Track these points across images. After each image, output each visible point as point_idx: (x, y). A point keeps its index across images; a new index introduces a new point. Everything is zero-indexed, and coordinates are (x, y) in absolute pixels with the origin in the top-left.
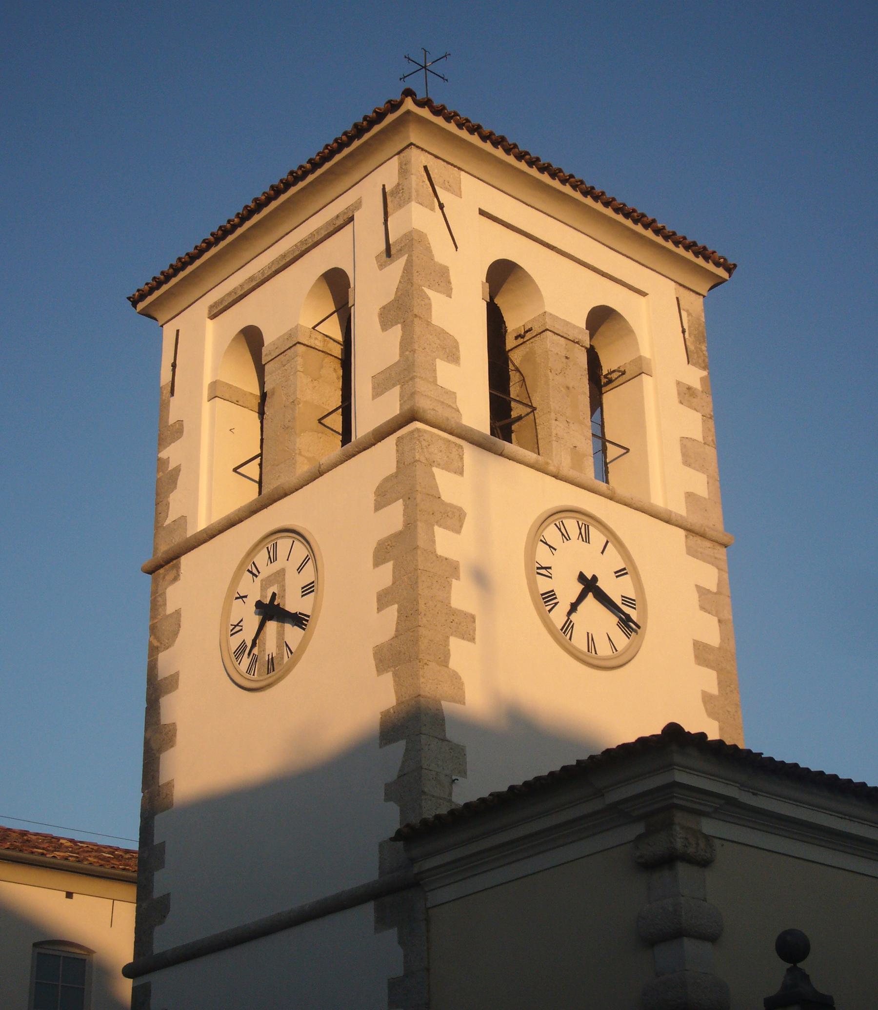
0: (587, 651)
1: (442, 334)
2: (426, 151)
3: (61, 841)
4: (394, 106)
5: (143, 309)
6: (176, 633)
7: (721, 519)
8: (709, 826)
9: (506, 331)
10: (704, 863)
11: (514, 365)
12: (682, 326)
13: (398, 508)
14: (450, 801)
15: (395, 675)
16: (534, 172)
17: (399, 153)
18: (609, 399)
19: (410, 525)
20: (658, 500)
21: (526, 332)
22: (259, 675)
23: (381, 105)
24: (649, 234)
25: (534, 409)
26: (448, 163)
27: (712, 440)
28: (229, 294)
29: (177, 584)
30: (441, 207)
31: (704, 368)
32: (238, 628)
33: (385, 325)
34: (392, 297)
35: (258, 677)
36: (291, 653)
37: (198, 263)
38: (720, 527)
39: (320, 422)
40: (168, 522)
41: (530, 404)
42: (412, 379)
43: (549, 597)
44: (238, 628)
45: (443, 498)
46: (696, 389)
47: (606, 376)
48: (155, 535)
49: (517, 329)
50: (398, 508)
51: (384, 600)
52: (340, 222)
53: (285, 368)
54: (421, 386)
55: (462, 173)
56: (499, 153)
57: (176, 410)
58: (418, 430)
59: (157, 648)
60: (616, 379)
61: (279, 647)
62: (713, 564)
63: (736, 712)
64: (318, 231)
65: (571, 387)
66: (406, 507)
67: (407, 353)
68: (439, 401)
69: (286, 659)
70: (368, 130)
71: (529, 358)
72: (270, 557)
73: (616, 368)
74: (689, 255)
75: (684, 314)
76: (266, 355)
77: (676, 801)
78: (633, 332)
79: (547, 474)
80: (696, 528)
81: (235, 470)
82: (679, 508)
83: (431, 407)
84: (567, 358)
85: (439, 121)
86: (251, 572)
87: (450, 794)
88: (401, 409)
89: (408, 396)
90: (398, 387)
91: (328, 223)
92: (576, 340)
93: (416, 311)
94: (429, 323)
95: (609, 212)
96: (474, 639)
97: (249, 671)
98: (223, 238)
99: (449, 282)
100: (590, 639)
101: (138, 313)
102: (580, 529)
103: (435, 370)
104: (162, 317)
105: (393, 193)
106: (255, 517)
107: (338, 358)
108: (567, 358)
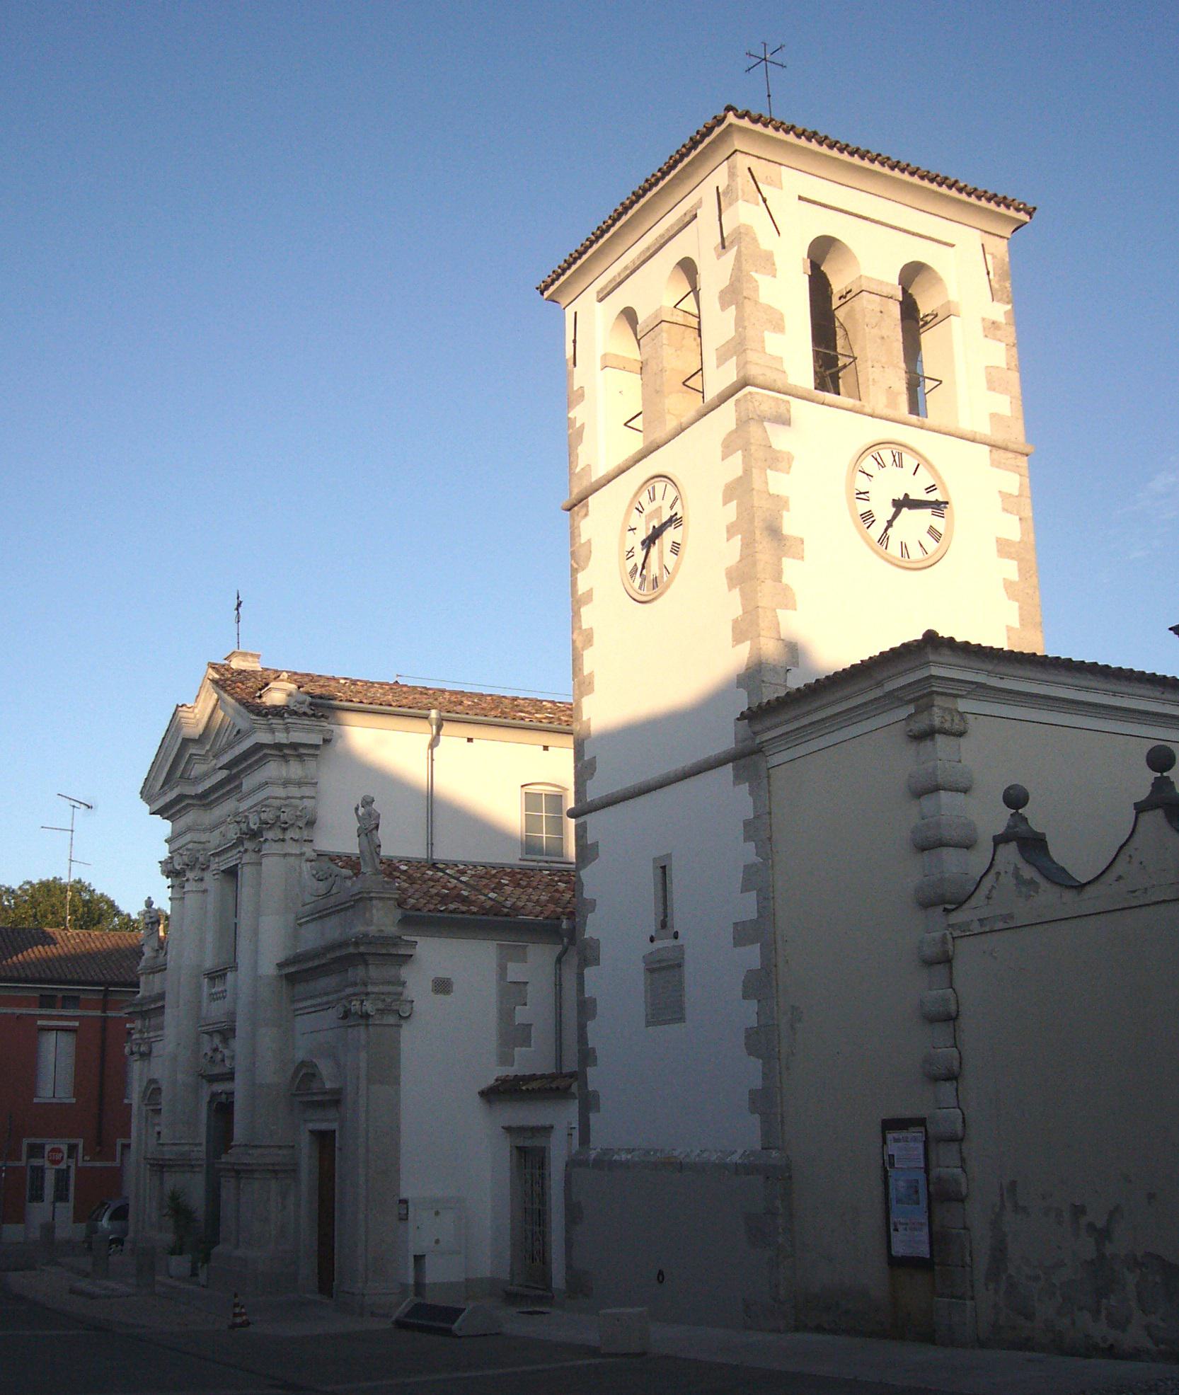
0: (900, 556)
1: (769, 309)
2: (749, 154)
3: (544, 703)
4: (720, 121)
5: (549, 296)
6: (589, 558)
7: (1023, 432)
8: (963, 705)
9: (832, 293)
10: (961, 734)
11: (840, 322)
12: (987, 269)
13: (738, 458)
14: (785, 686)
15: (741, 590)
16: (845, 156)
17: (727, 158)
18: (927, 339)
19: (747, 472)
20: (966, 426)
21: (848, 293)
22: (648, 591)
23: (710, 122)
24: (953, 193)
25: (855, 359)
26: (769, 161)
27: (1016, 365)
28: (610, 282)
29: (588, 518)
30: (765, 201)
31: (1008, 303)
32: (631, 554)
33: (724, 306)
34: (728, 283)
35: (647, 593)
36: (669, 573)
37: (585, 257)
38: (1022, 439)
39: (685, 385)
40: (578, 470)
41: (852, 355)
42: (745, 350)
43: (868, 517)
44: (631, 554)
45: (773, 447)
46: (1001, 323)
47: (922, 320)
48: (570, 480)
49: (839, 291)
50: (738, 458)
51: (731, 531)
52: (687, 219)
53: (655, 342)
54: (752, 356)
55: (783, 168)
56: (813, 145)
57: (580, 377)
58: (750, 393)
59: (576, 569)
60: (931, 321)
61: (660, 569)
62: (1015, 472)
63: (1034, 593)
64: (672, 226)
65: (885, 337)
66: (744, 456)
67: (740, 329)
68: (767, 366)
69: (665, 579)
70: (701, 142)
71: (850, 315)
72: (650, 498)
73: (930, 312)
74: (992, 206)
75: (988, 257)
76: (640, 332)
77: (935, 689)
78: (941, 280)
79: (865, 414)
80: (999, 443)
81: (625, 425)
82: (984, 428)
83: (761, 373)
84: (881, 312)
85: (758, 127)
86: (638, 509)
87: (785, 681)
88: (737, 377)
89: (742, 366)
90: (735, 358)
91: (679, 220)
92: (890, 296)
93: (745, 294)
94: (756, 302)
95: (915, 180)
96: (803, 557)
97: (640, 588)
98: (602, 236)
99: (774, 264)
100: (904, 547)
101: (546, 299)
102: (894, 456)
103: (763, 341)
104: (564, 302)
105: (725, 193)
106: (637, 465)
107: (695, 328)
108: (881, 312)
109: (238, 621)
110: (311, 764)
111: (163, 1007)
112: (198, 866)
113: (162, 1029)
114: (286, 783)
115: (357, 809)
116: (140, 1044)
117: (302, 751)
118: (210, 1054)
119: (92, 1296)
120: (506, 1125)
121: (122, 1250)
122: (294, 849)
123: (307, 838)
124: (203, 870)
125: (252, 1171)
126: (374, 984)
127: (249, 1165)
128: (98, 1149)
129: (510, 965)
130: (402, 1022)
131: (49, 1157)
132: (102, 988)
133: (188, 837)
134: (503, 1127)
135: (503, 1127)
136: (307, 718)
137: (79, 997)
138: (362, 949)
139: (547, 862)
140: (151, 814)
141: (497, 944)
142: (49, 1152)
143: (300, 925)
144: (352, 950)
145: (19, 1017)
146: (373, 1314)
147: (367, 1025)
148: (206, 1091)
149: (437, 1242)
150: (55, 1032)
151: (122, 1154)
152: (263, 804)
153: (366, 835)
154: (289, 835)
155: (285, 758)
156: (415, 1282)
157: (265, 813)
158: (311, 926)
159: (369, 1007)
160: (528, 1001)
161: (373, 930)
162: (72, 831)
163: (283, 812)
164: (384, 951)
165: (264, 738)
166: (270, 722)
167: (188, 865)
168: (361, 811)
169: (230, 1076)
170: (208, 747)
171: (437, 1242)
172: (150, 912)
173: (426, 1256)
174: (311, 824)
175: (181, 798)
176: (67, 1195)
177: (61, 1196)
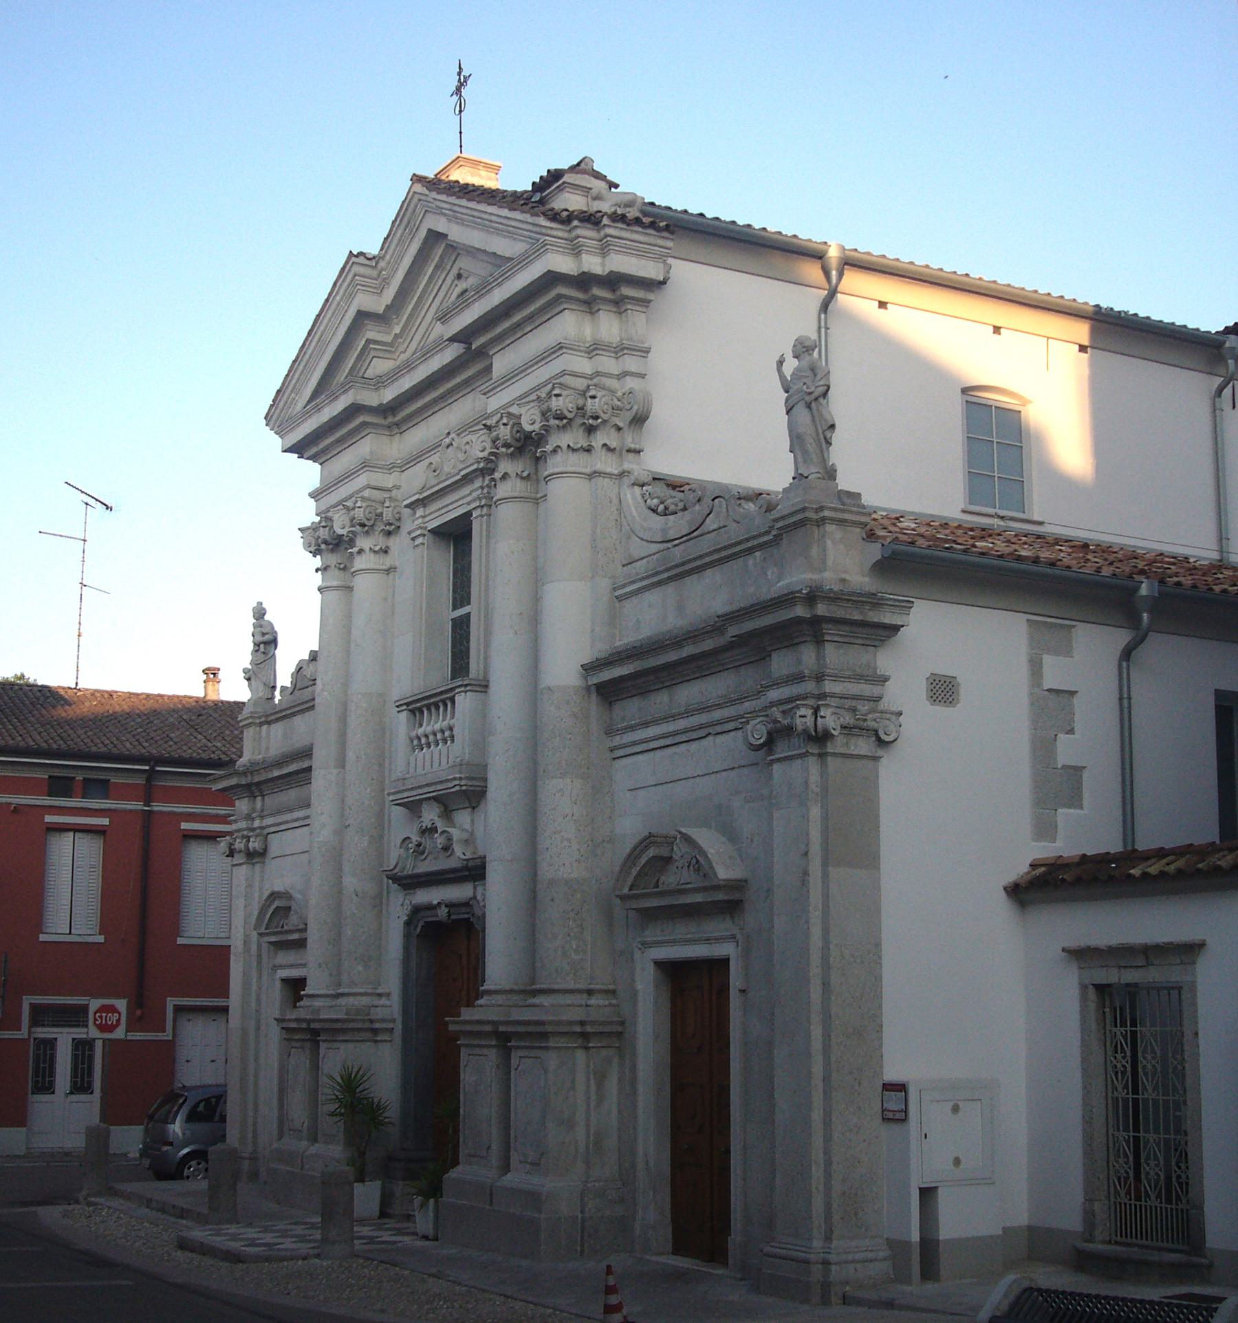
109: (460, 111)
110: (637, 321)
111: (309, 769)
112: (380, 526)
113: (309, 806)
114: (594, 349)
115: (780, 363)
116: (248, 838)
117: (626, 291)
118: (415, 839)
119: (234, 1258)
120: (1073, 944)
121: (206, 1170)
122: (607, 464)
123: (633, 446)
124: (389, 533)
125: (544, 1036)
126: (837, 678)
127: (542, 1023)
128: (138, 1012)
129: (1048, 660)
130: (880, 753)
131: (95, 1020)
132: (147, 768)
133: (361, 480)
134: (1064, 950)
135: (1064, 950)
136: (640, 229)
137: (109, 780)
138: (821, 609)
139: (1002, 518)
140: (285, 451)
141: (1028, 620)
142: (95, 1013)
143: (619, 599)
144: (800, 611)
145: (17, 809)
146: (845, 1300)
147: (822, 756)
148: (399, 906)
149: (957, 1161)
150: (71, 834)
151: (175, 1021)
152: (555, 385)
153: (809, 406)
154: (599, 439)
155: (590, 306)
156: (920, 1238)
157: (561, 398)
158: (653, 597)
159: (830, 720)
160: (1077, 727)
161: (829, 579)
162: (85, 541)
163: (593, 397)
164: (857, 616)
165: (563, 264)
166: (574, 234)
167: (363, 525)
168: (791, 365)
169: (475, 872)
170: (397, 330)
171: (957, 1161)
172: (261, 626)
173: (940, 1191)
174: (639, 420)
175: (354, 410)
176: (90, 1084)
177: (81, 1085)
